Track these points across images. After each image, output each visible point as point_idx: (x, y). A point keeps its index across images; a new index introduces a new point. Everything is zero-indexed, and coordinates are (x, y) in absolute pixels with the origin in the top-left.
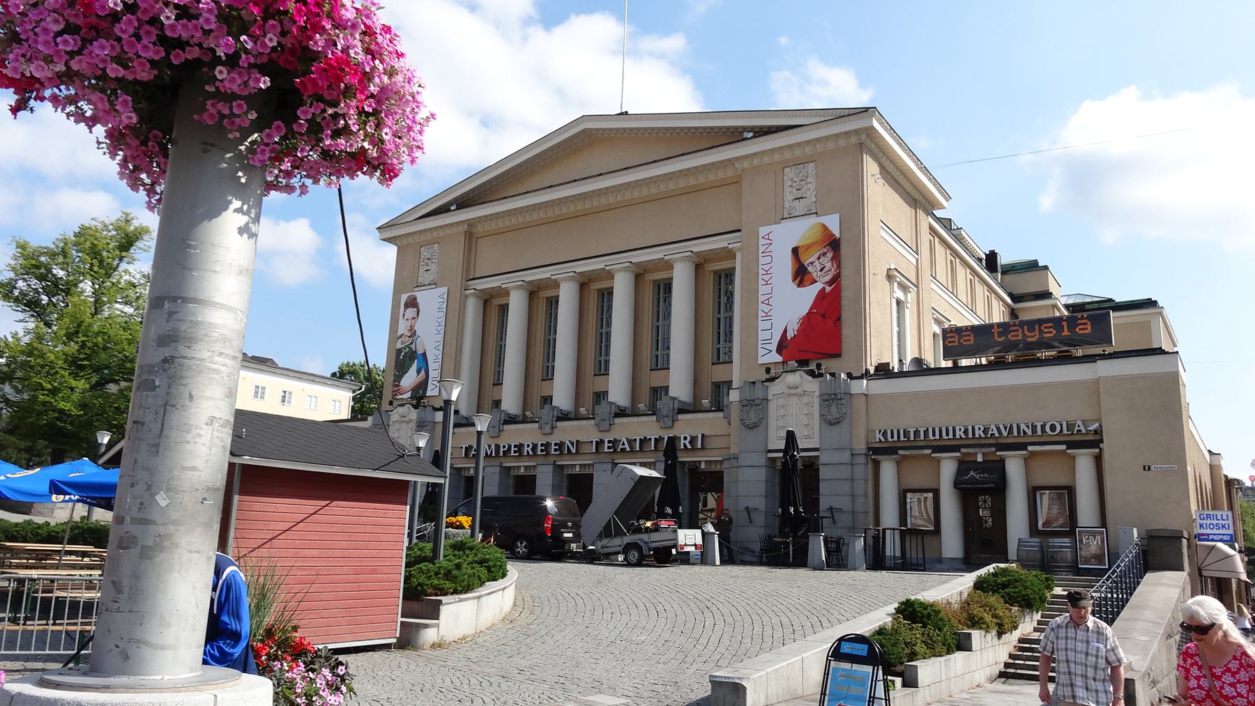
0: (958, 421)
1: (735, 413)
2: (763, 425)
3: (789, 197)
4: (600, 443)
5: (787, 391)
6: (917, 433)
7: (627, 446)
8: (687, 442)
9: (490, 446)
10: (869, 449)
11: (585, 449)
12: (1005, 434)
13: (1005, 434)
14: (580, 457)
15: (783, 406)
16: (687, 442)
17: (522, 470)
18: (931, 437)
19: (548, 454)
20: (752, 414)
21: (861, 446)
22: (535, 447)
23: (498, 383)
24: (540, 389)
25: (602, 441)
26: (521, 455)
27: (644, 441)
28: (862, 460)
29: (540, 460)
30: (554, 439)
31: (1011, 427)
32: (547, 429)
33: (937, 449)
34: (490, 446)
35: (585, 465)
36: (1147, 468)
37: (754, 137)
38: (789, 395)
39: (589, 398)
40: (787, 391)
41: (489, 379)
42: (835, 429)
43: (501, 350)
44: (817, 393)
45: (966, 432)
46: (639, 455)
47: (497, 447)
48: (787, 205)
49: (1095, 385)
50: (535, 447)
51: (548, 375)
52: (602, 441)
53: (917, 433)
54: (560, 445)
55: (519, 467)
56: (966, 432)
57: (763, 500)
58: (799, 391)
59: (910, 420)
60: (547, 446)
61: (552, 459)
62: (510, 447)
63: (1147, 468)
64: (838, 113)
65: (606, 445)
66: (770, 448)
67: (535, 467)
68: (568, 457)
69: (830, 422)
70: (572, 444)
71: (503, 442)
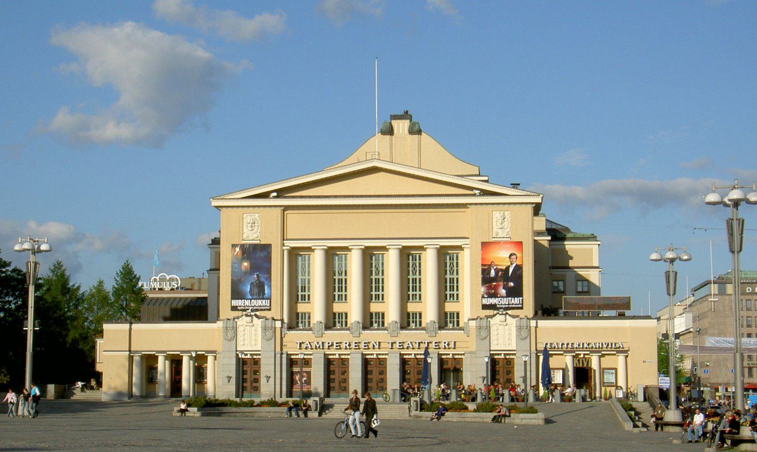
7: (309, 346)
8: (446, 345)
16: (446, 345)
32: (357, 334)
34: (318, 343)
38: (246, 326)
44: (260, 326)
69: (520, 338)
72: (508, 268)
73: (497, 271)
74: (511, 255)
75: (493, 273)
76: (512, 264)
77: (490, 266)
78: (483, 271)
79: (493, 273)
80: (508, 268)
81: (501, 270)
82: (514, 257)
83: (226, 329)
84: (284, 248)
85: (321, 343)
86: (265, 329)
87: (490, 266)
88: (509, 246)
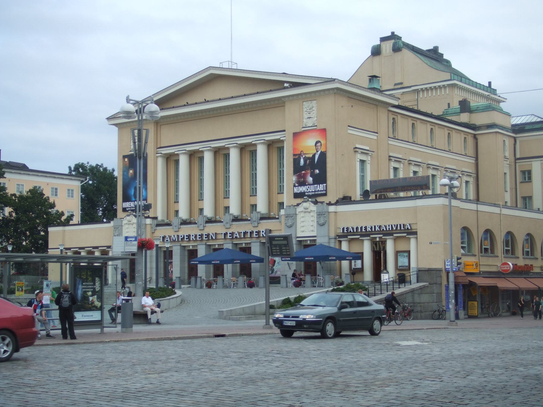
0: (369, 223)
1: (283, 219)
2: (294, 226)
3: (306, 116)
4: (226, 234)
5: (304, 210)
6: (357, 228)
7: (168, 239)
9: (174, 236)
10: (337, 236)
11: (219, 237)
12: (394, 228)
13: (394, 228)
14: (218, 241)
15: (303, 217)
16: (263, 233)
17: (244, 245)
18: (363, 230)
19: (202, 240)
20: (290, 221)
21: (333, 235)
22: (196, 236)
23: (201, 199)
24: (197, 205)
25: (227, 233)
26: (190, 240)
27: (245, 233)
28: (333, 241)
29: (199, 243)
30: (205, 233)
31: (397, 225)
32: (201, 228)
33: (362, 236)
34: (174, 236)
35: (247, 243)
36: (431, 243)
37: (291, 87)
39: (275, 206)
40: (304, 210)
41: (172, 199)
42: (323, 227)
43: (201, 181)
45: (371, 228)
46: (243, 239)
47: (178, 236)
48: (305, 120)
49: (415, 208)
50: (196, 236)
51: (254, 193)
52: (227, 233)
53: (357, 228)
54: (208, 235)
55: (189, 246)
56: (371, 228)
57: (229, 265)
58: (309, 210)
59: (352, 224)
60: (201, 236)
61: (204, 242)
62: (184, 237)
63: (431, 243)
64: (329, 80)
65: (255, 233)
66: (298, 236)
67: (197, 246)
68: (211, 241)
70: (213, 234)
71: (181, 234)
72: (314, 155)
73: (305, 159)
74: (317, 143)
75: (302, 162)
76: (317, 152)
77: (300, 155)
78: (295, 160)
79: (302, 162)
80: (314, 155)
81: (309, 158)
82: (319, 144)
83: (116, 228)
84: (157, 155)
85: (176, 236)
86: (320, 214)
87: (300, 155)
88: (314, 134)
